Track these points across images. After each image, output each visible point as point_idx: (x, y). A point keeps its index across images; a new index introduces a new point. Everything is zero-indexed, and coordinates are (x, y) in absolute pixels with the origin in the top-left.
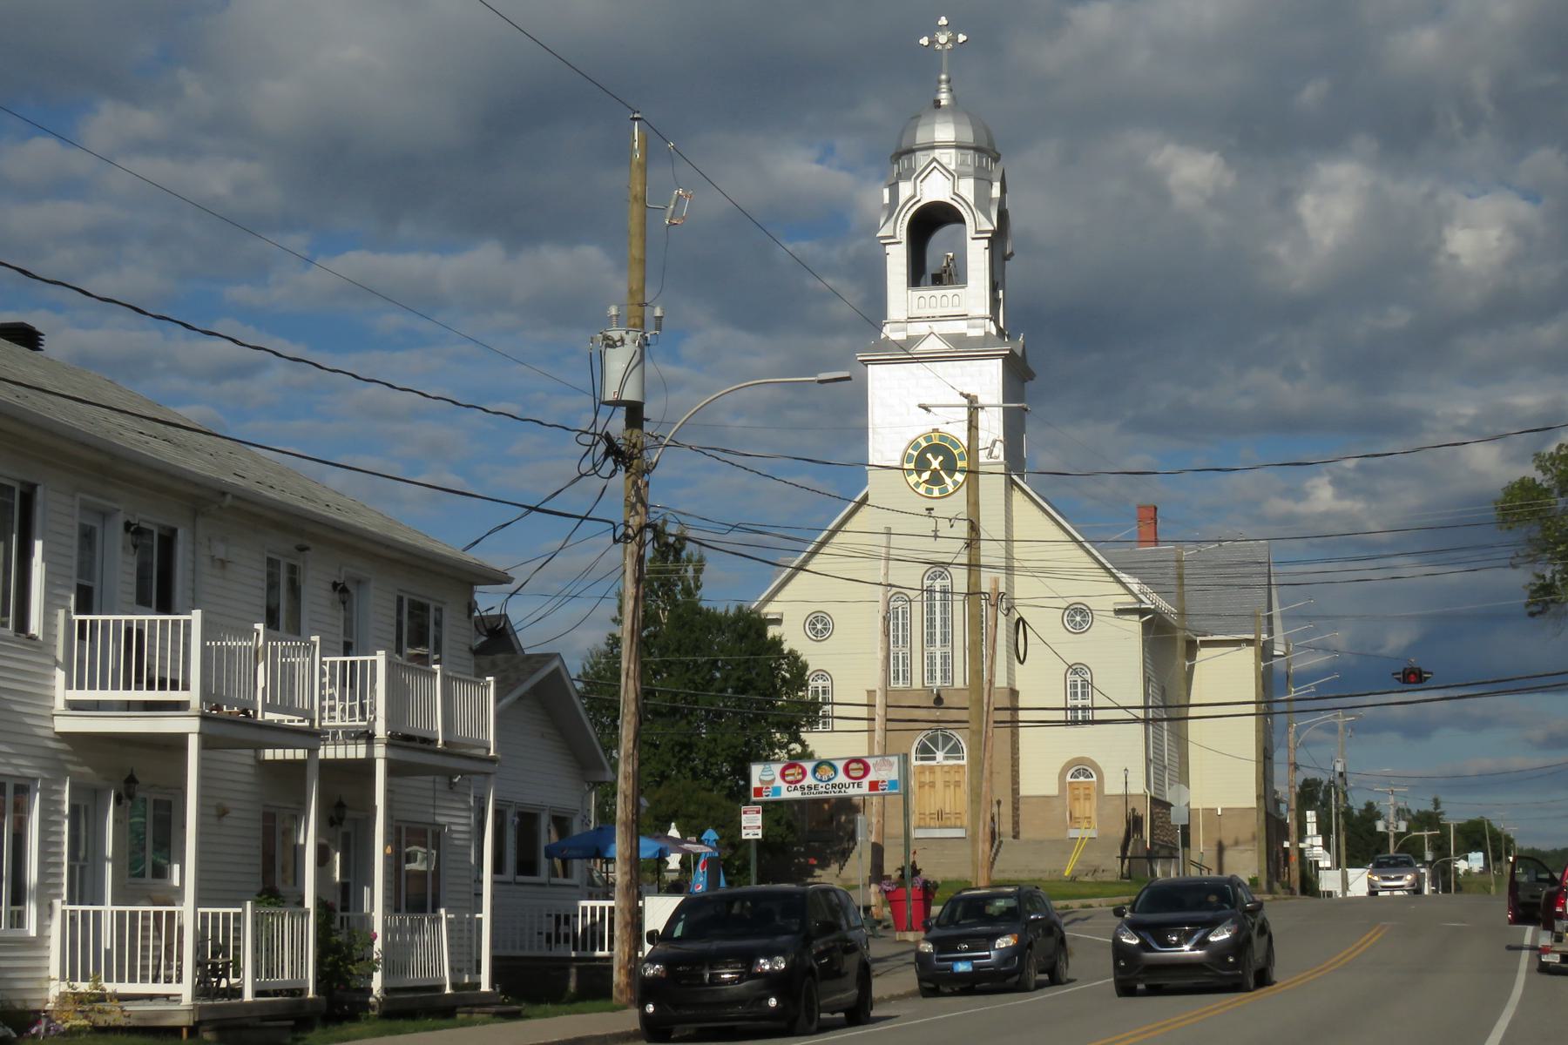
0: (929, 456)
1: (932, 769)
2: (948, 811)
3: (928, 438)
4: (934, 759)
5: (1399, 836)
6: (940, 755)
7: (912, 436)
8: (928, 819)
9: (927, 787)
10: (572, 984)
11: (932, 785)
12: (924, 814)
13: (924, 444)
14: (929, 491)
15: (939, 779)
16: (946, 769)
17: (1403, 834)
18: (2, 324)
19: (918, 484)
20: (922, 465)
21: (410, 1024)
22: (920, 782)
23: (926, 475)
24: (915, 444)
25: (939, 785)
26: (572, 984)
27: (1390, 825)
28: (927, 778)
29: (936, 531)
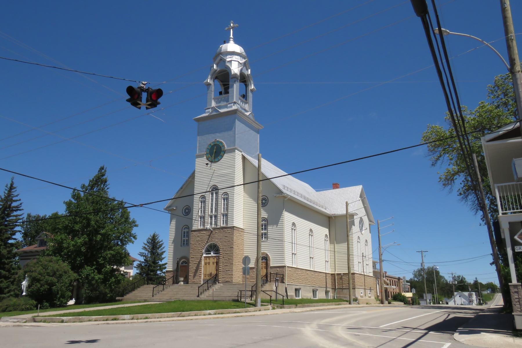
11: (209, 263)
25: (211, 263)
28: (208, 261)
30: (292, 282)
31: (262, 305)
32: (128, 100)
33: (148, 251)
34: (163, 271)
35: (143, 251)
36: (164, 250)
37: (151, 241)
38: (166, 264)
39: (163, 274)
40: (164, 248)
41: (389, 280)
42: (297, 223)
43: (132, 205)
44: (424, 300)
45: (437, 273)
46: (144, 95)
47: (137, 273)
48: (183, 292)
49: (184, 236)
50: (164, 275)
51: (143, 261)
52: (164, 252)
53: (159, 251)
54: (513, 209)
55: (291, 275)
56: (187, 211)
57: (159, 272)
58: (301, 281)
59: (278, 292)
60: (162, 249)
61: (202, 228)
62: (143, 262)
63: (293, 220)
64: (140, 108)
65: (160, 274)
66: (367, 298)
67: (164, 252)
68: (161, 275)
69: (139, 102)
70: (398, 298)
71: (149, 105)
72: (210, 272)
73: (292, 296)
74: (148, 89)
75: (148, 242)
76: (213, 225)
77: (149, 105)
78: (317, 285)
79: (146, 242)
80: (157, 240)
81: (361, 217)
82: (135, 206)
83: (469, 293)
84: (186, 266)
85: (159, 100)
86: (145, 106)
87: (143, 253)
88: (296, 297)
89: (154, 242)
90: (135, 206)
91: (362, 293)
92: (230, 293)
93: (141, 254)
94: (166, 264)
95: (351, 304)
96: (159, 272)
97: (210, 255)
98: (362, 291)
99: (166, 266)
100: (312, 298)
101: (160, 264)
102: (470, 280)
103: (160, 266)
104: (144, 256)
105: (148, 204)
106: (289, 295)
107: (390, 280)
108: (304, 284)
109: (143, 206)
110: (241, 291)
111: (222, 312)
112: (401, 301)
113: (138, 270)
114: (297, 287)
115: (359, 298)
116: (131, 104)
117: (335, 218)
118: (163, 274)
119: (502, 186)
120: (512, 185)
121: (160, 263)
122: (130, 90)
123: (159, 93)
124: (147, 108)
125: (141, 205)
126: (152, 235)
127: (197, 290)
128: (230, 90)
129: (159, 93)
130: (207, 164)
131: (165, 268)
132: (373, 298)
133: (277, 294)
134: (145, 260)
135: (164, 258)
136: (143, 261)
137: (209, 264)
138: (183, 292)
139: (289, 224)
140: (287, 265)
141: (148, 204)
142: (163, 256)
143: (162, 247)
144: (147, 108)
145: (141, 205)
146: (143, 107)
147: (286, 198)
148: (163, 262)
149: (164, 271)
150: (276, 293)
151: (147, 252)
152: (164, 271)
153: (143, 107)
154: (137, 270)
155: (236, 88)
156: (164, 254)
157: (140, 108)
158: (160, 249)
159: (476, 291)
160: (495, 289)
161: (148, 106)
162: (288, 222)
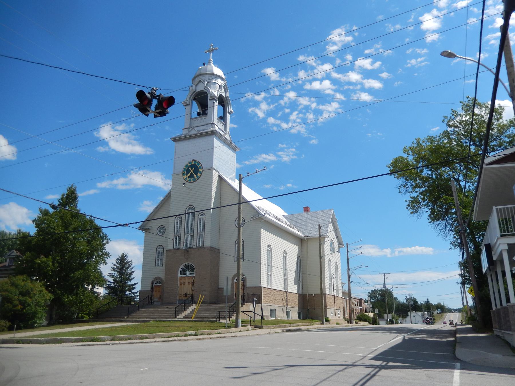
0: (190, 168)
1: (184, 277)
2: (189, 294)
3: (190, 163)
4: (186, 274)
5: (412, 305)
6: (188, 273)
7: (185, 163)
8: (182, 297)
9: (183, 285)
10: (279, 115)
11: (184, 284)
12: (181, 295)
13: (189, 165)
14: (190, 180)
15: (187, 281)
16: (189, 278)
17: (413, 305)
18: (514, 236)
19: (186, 178)
20: (188, 171)
21: (82, 324)
22: (181, 283)
23: (189, 175)
24: (187, 165)
25: (187, 283)
26: (279, 115)
27: (454, 323)
28: (183, 281)
29: (287, 294)
30: (267, 302)
31: (242, 326)
32: (136, 106)
33: (117, 272)
34: (133, 292)
35: (113, 272)
36: (133, 270)
37: (120, 261)
38: (135, 284)
39: (132, 294)
40: (133, 268)
41: (356, 302)
42: (272, 245)
43: (117, 225)
44: (384, 320)
45: (390, 294)
46: (155, 102)
47: (106, 293)
48: (158, 312)
49: (159, 256)
50: (133, 296)
51: (112, 281)
52: (133, 272)
53: (128, 271)
54: (508, 232)
55: (267, 296)
56: (162, 231)
57: (128, 292)
58: (275, 301)
59: (256, 312)
60: (131, 269)
61: (177, 248)
62: (112, 282)
63: (269, 241)
64: (147, 115)
65: (130, 294)
66: (337, 318)
67: (133, 272)
68: (131, 295)
69: (148, 109)
70: (361, 318)
71: (158, 113)
72: (186, 293)
73: (267, 316)
74: (159, 96)
75: (117, 263)
76: (189, 245)
77: (158, 113)
78: (290, 306)
79: (115, 263)
80: (126, 261)
81: (331, 240)
82: (120, 225)
83: (423, 313)
84: (160, 286)
85: (169, 110)
86: (153, 114)
87: (112, 274)
88: (271, 317)
89: (123, 262)
90: (120, 225)
91: (332, 313)
92: (172, 312)
93: (111, 275)
94: (135, 284)
95: (324, 324)
96: (128, 292)
97: (185, 276)
98: (333, 311)
99: (135, 286)
100: (285, 318)
101: (129, 285)
102: (421, 301)
103: (130, 286)
104: (113, 277)
105: (134, 223)
106: (265, 316)
107: (357, 302)
108: (279, 304)
109: (129, 225)
110: (220, 311)
111: (209, 333)
112: (365, 320)
113: (107, 290)
114: (272, 308)
115: (330, 318)
116: (139, 111)
117: (307, 240)
118: (132, 295)
119: (500, 209)
120: (503, 208)
121: (129, 283)
122: (140, 95)
123: (171, 101)
124: (155, 116)
125: (127, 225)
126: (121, 256)
127: (173, 310)
128: (209, 111)
129: (171, 101)
130: (184, 184)
131: (134, 288)
132: (342, 318)
133: (255, 314)
134: (114, 280)
135: (133, 278)
136: (112, 281)
137: (184, 284)
138: (158, 312)
139: (265, 245)
140: (263, 286)
141: (134, 223)
142: (132, 277)
143: (131, 267)
144: (155, 116)
145: (127, 225)
146: (151, 115)
147: (263, 219)
148: (132, 282)
149: (133, 291)
150: (254, 313)
151: (116, 273)
152: (133, 291)
153: (151, 115)
154: (106, 290)
155: (215, 109)
156: (134, 274)
157: (147, 115)
158: (129, 269)
159: (428, 311)
160: (30, 290)
161: (157, 114)
162: (264, 243)
